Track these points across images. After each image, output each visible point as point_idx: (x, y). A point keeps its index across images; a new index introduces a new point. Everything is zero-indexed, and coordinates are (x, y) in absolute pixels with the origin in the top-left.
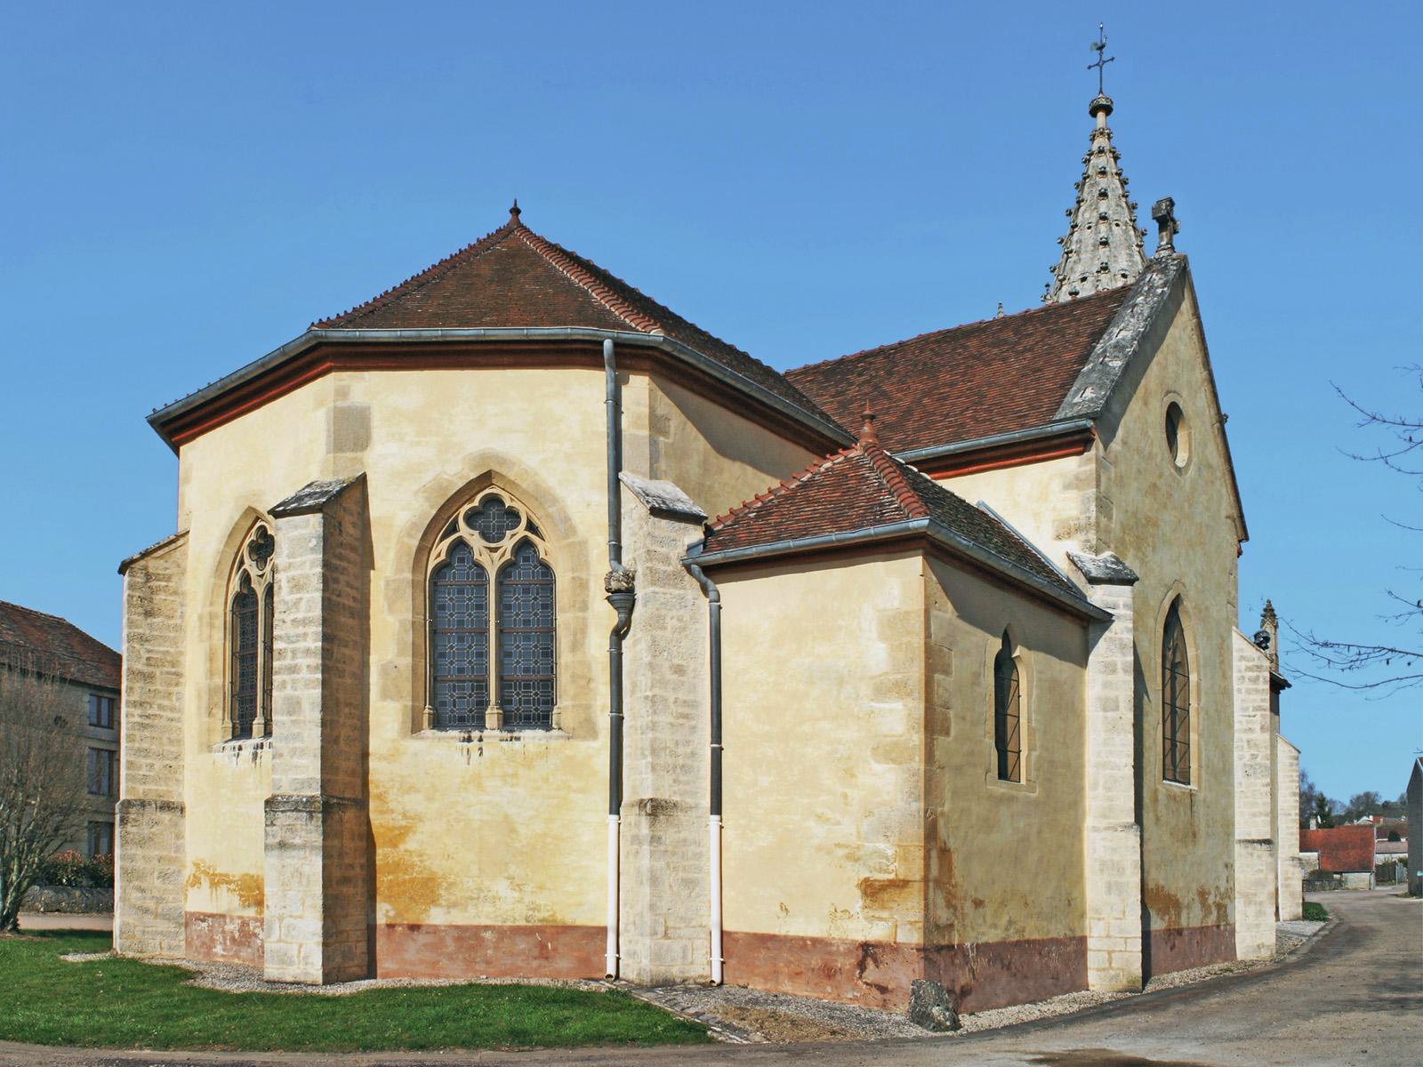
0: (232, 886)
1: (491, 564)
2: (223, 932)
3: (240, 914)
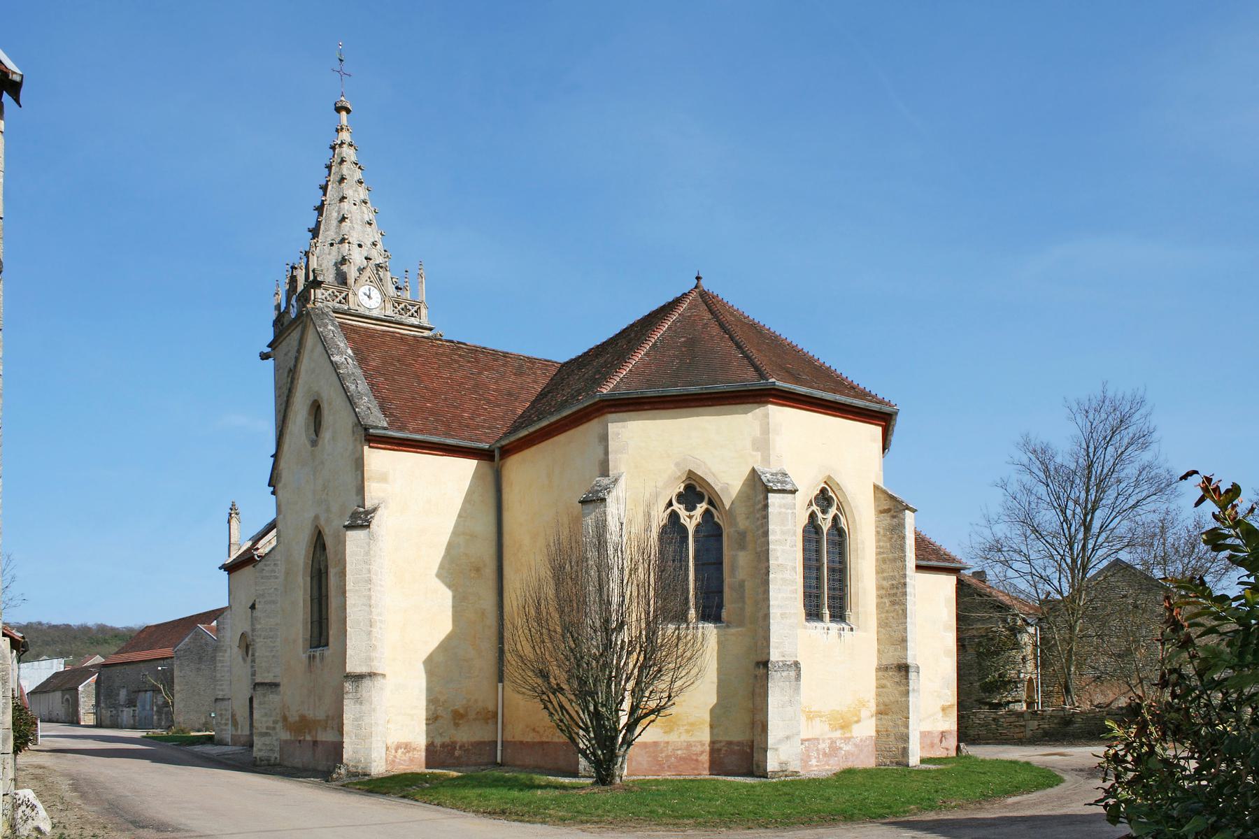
0: (824, 719)
1: (691, 526)
2: (818, 750)
3: (829, 736)
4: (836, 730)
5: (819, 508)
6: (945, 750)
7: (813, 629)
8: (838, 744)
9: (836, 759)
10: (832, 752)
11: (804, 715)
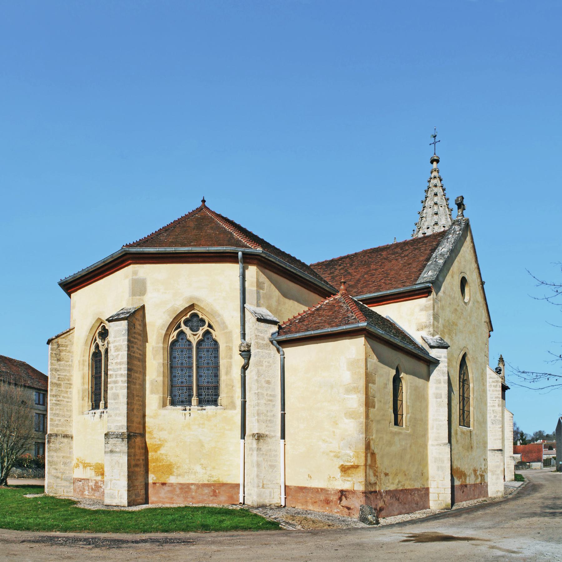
0: (92, 468)
2: (88, 486)
3: (95, 479)
4: (98, 475)
5: (201, 328)
6: (346, 510)
7: (86, 414)
8: (99, 484)
9: (99, 493)
10: (96, 489)
11: (82, 465)
